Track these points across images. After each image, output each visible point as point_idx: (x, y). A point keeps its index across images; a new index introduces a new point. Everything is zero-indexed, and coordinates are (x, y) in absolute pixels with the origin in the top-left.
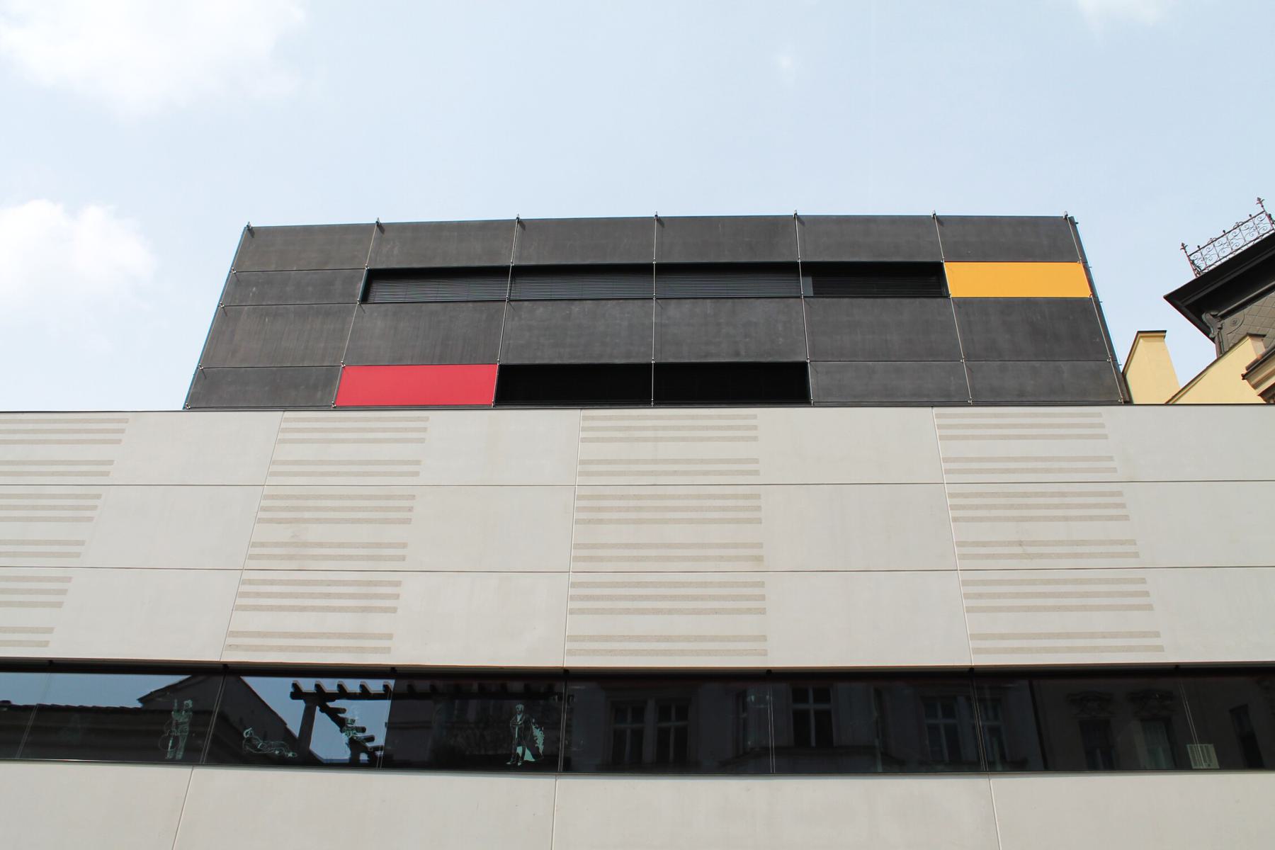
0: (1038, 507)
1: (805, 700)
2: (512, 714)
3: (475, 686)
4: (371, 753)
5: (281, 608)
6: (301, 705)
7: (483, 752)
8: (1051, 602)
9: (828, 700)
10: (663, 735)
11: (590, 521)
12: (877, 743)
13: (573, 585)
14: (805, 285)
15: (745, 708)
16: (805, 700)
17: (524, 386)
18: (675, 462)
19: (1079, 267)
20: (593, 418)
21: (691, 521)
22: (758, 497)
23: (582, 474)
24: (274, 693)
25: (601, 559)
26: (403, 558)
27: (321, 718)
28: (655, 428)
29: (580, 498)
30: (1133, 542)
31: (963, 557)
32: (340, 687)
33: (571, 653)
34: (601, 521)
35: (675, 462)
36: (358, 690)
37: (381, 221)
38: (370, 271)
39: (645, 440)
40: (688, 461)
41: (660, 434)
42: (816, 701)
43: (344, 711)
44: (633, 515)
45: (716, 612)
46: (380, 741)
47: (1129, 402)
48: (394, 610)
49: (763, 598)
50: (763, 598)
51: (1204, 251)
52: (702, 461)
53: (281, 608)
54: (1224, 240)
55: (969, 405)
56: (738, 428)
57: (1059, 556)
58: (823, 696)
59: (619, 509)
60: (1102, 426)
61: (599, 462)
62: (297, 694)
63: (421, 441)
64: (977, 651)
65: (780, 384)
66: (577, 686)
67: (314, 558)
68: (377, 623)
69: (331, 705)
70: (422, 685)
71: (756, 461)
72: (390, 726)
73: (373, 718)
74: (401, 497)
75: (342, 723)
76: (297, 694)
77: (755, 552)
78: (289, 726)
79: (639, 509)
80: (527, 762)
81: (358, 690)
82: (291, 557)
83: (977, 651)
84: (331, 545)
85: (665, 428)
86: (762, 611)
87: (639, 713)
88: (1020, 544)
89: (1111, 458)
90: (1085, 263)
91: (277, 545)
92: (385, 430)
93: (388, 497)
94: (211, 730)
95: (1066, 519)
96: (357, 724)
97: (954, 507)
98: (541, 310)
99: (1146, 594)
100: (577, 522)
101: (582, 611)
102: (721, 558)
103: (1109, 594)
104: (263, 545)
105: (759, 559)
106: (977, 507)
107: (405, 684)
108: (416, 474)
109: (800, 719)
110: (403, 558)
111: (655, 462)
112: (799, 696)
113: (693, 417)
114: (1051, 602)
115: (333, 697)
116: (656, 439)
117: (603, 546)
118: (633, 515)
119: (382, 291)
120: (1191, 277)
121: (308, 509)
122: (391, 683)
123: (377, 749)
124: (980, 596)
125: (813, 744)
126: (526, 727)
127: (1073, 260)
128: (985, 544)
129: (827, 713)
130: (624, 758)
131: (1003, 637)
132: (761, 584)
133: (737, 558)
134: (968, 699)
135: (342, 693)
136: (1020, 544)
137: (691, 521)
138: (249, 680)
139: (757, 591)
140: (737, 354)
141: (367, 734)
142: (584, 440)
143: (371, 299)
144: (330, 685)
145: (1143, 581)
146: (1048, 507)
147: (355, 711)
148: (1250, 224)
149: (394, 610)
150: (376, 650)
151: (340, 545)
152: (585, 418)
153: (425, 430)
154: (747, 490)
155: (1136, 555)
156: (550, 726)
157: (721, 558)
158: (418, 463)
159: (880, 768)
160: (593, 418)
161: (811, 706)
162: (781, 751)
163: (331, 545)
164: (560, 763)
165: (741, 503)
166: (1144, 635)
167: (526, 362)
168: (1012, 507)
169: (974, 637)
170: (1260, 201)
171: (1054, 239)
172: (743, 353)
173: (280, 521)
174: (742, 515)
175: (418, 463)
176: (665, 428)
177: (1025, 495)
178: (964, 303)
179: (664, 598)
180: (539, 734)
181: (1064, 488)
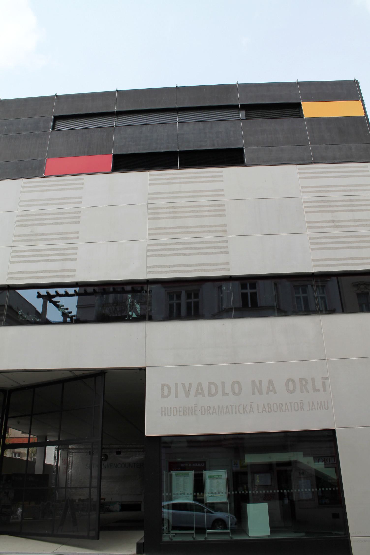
0: (341, 206)
1: (246, 288)
2: (127, 299)
3: (111, 289)
4: (71, 318)
5: (29, 261)
6: (41, 300)
7: (116, 315)
9: (255, 288)
11: (154, 219)
12: (275, 304)
13: (149, 245)
14: (242, 114)
15: (221, 293)
16: (246, 288)
17: (125, 162)
18: (189, 192)
19: (360, 102)
20: (154, 175)
21: (197, 217)
22: (224, 205)
23: (150, 199)
24: (30, 296)
25: (160, 234)
26: (77, 238)
27: (50, 305)
28: (180, 178)
29: (150, 209)
31: (310, 228)
32: (56, 292)
33: (149, 273)
34: (159, 218)
35: (189, 192)
36: (64, 293)
37: (58, 94)
40: (194, 192)
41: (182, 180)
42: (247, 289)
43: (59, 302)
44: (172, 215)
45: (25, 262)
46: (74, 313)
48: (75, 259)
49: (227, 247)
52: (200, 191)
53: (29, 261)
55: (312, 164)
56: (215, 177)
57: (349, 226)
58: (253, 286)
59: (166, 213)
62: (39, 296)
63: (82, 188)
64: (315, 266)
65: (232, 157)
66: (153, 287)
67: (41, 240)
68: (69, 265)
69: (53, 299)
70: (90, 290)
72: (78, 307)
73: (71, 304)
74: (75, 213)
75: (58, 306)
76: (39, 296)
77: (224, 228)
78: (37, 309)
79: (175, 212)
80: (134, 318)
81: (64, 293)
82: (31, 240)
83: (315, 266)
85: (184, 178)
86: (227, 253)
87: (179, 297)
88: (333, 221)
90: (362, 101)
91: (24, 235)
92: (66, 185)
93: (69, 213)
94: (5, 312)
95: (352, 211)
96: (65, 307)
97: (306, 207)
98: (129, 130)
100: (149, 219)
101: (153, 256)
102: (209, 231)
104: (19, 236)
105: (225, 231)
106: (316, 207)
107: (83, 289)
108: (81, 202)
109: (244, 296)
110: (77, 238)
111: (180, 192)
112: (244, 287)
113: (196, 173)
115: (54, 296)
116: (180, 183)
118: (172, 215)
119: (61, 125)
121: (37, 220)
122: (77, 289)
123: (73, 316)
124: (317, 243)
125: (250, 306)
126: (133, 304)
128: (318, 222)
129: (255, 293)
130: (173, 314)
131: (326, 260)
132: (227, 242)
133: (216, 231)
134: (312, 286)
135: (58, 295)
136: (333, 221)
137: (197, 217)
138: (19, 291)
139: (225, 244)
140: (214, 145)
141: (69, 310)
142: (150, 184)
143: (56, 129)
144: (52, 291)
146: (344, 206)
147: (62, 301)
149: (75, 259)
150: (69, 276)
151: (51, 234)
152: (150, 175)
153: (83, 184)
154: (219, 203)
156: (143, 303)
157: (209, 231)
158: (81, 198)
159: (276, 314)
160: (154, 175)
161: (249, 291)
162: (236, 309)
164: (147, 318)
165: (217, 208)
167: (124, 153)
168: (330, 206)
169: (314, 260)
172: (216, 145)
173: (25, 226)
174: (218, 213)
175: (81, 198)
176: (184, 178)
177: (336, 201)
178: (311, 120)
180: (138, 306)
181: (352, 198)
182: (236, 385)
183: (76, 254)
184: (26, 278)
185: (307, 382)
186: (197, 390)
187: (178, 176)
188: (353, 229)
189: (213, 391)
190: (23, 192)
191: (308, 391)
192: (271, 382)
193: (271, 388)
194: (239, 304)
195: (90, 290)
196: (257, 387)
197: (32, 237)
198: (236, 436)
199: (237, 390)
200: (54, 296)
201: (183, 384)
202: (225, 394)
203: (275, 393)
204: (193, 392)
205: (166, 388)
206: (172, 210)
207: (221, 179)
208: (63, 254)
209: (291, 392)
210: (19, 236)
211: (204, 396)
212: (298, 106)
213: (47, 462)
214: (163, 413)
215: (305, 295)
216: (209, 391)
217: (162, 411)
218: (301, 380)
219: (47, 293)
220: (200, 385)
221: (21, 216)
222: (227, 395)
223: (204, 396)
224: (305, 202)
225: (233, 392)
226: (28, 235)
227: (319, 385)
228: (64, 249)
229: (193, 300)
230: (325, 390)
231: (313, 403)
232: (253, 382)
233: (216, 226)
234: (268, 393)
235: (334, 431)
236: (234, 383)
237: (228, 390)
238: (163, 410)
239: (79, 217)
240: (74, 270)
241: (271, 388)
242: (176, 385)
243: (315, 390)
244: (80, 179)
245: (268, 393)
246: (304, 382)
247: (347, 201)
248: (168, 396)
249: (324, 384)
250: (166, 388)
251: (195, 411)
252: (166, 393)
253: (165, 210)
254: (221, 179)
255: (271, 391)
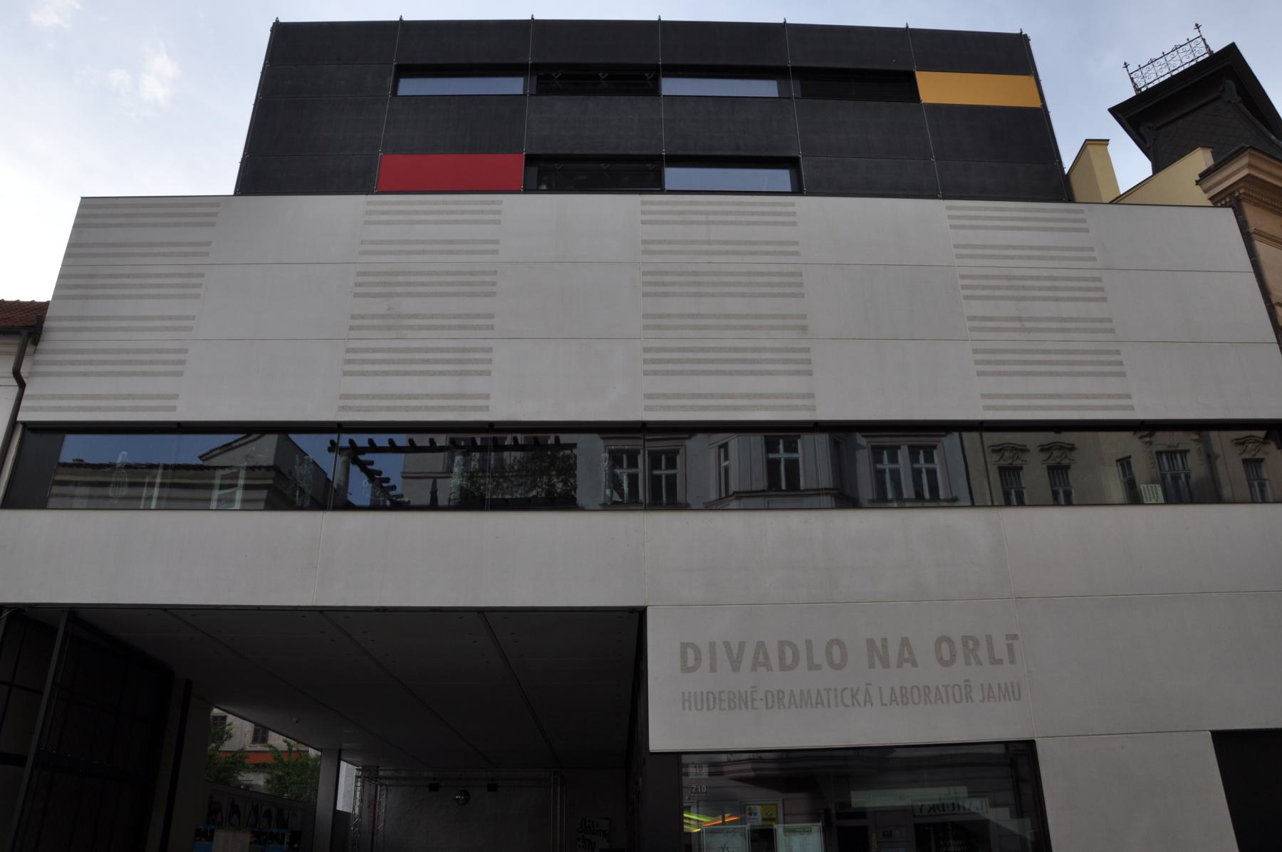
0: (1033, 288)
5: (386, 373)
6: (341, 459)
8: (1044, 368)
10: (655, 481)
11: (655, 295)
15: (726, 458)
18: (726, 243)
20: (652, 203)
21: (743, 295)
22: (800, 274)
23: (644, 252)
24: (315, 447)
27: (354, 469)
28: (707, 213)
29: (644, 274)
30: (1110, 320)
31: (973, 329)
34: (665, 295)
36: (428, 444)
38: (397, 66)
39: (699, 223)
41: (711, 218)
43: (372, 463)
44: (693, 289)
45: (376, 373)
47: (1071, 199)
49: (809, 361)
50: (490, 361)
51: (1144, 70)
53: (386, 373)
54: (1162, 61)
60: (1084, 221)
61: (660, 242)
62: (333, 447)
68: (474, 385)
69: (362, 458)
71: (797, 243)
76: (333, 447)
79: (699, 284)
81: (428, 444)
82: (389, 328)
84: (424, 316)
85: (715, 213)
87: (633, 463)
88: (1020, 319)
89: (1091, 249)
91: (374, 317)
95: (1057, 299)
97: (964, 287)
99: (1121, 363)
100: (645, 295)
101: (656, 373)
103: (1092, 363)
104: (362, 317)
108: (496, 252)
109: (772, 466)
110: (492, 327)
111: (708, 242)
112: (771, 446)
114: (1044, 368)
115: (363, 451)
117: (669, 316)
120: (1131, 93)
124: (988, 362)
125: (784, 487)
127: (1027, 74)
128: (991, 319)
132: (807, 350)
135: (373, 448)
136: (1020, 319)
137: (743, 295)
139: (803, 356)
141: (391, 483)
144: (362, 440)
145: (1118, 352)
146: (1041, 288)
148: (1187, 47)
149: (488, 373)
151: (433, 316)
152: (643, 203)
155: (1112, 331)
158: (496, 242)
160: (652, 203)
163: (424, 316)
165: (785, 279)
166: (1120, 396)
170: (1197, 27)
171: (1009, 54)
173: (376, 296)
176: (715, 213)
179: (699, 361)
182: (836, 649)
183: (490, 361)
184: (381, 409)
185: (976, 642)
186: (756, 658)
187: (425, 208)
188: (1059, 336)
189: (789, 660)
190: (367, 223)
191: (979, 663)
192: (905, 643)
193: (906, 655)
194: (761, 484)
195: (422, 440)
196: (877, 653)
197: (391, 322)
198: (952, 751)
199: (837, 658)
200: (363, 451)
201: (727, 645)
202: (812, 666)
203: (915, 664)
204: (747, 661)
205: (690, 651)
206: (692, 279)
207: (792, 219)
208: (460, 361)
209: (946, 664)
210: (362, 317)
211: (770, 669)
212: (908, 81)
213: (340, 807)
214: (687, 704)
215: (894, 466)
216: (780, 658)
217: (684, 701)
218: (965, 639)
219: (351, 442)
220: (761, 645)
221: (364, 274)
222: (818, 667)
223: (770, 669)
224: (963, 277)
225: (831, 663)
226: (382, 317)
227: (1001, 651)
228: (464, 350)
229: (663, 472)
230: (1012, 661)
231: (990, 687)
232: (870, 642)
233: (784, 317)
234: (899, 665)
235: (1030, 746)
236: (831, 643)
237: (820, 657)
238: (686, 697)
239: (494, 284)
240: (487, 397)
241: (906, 655)
242: (712, 645)
243: (995, 661)
244: (493, 202)
245: (899, 665)
246: (970, 643)
247: (1045, 278)
248: (695, 668)
249: (1010, 649)
250: (690, 651)
251: (753, 700)
252: (691, 662)
253: (677, 279)
254: (792, 219)
255: (907, 660)
